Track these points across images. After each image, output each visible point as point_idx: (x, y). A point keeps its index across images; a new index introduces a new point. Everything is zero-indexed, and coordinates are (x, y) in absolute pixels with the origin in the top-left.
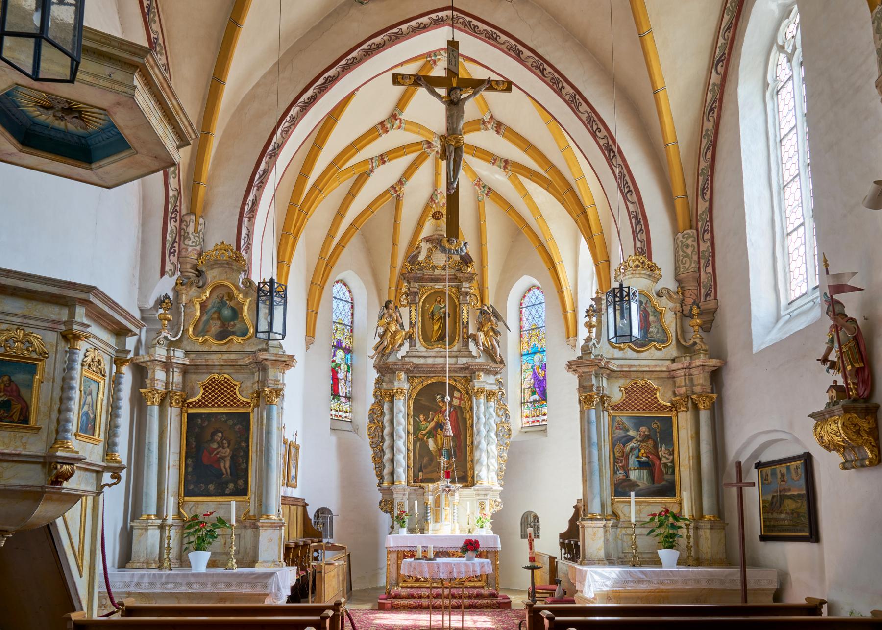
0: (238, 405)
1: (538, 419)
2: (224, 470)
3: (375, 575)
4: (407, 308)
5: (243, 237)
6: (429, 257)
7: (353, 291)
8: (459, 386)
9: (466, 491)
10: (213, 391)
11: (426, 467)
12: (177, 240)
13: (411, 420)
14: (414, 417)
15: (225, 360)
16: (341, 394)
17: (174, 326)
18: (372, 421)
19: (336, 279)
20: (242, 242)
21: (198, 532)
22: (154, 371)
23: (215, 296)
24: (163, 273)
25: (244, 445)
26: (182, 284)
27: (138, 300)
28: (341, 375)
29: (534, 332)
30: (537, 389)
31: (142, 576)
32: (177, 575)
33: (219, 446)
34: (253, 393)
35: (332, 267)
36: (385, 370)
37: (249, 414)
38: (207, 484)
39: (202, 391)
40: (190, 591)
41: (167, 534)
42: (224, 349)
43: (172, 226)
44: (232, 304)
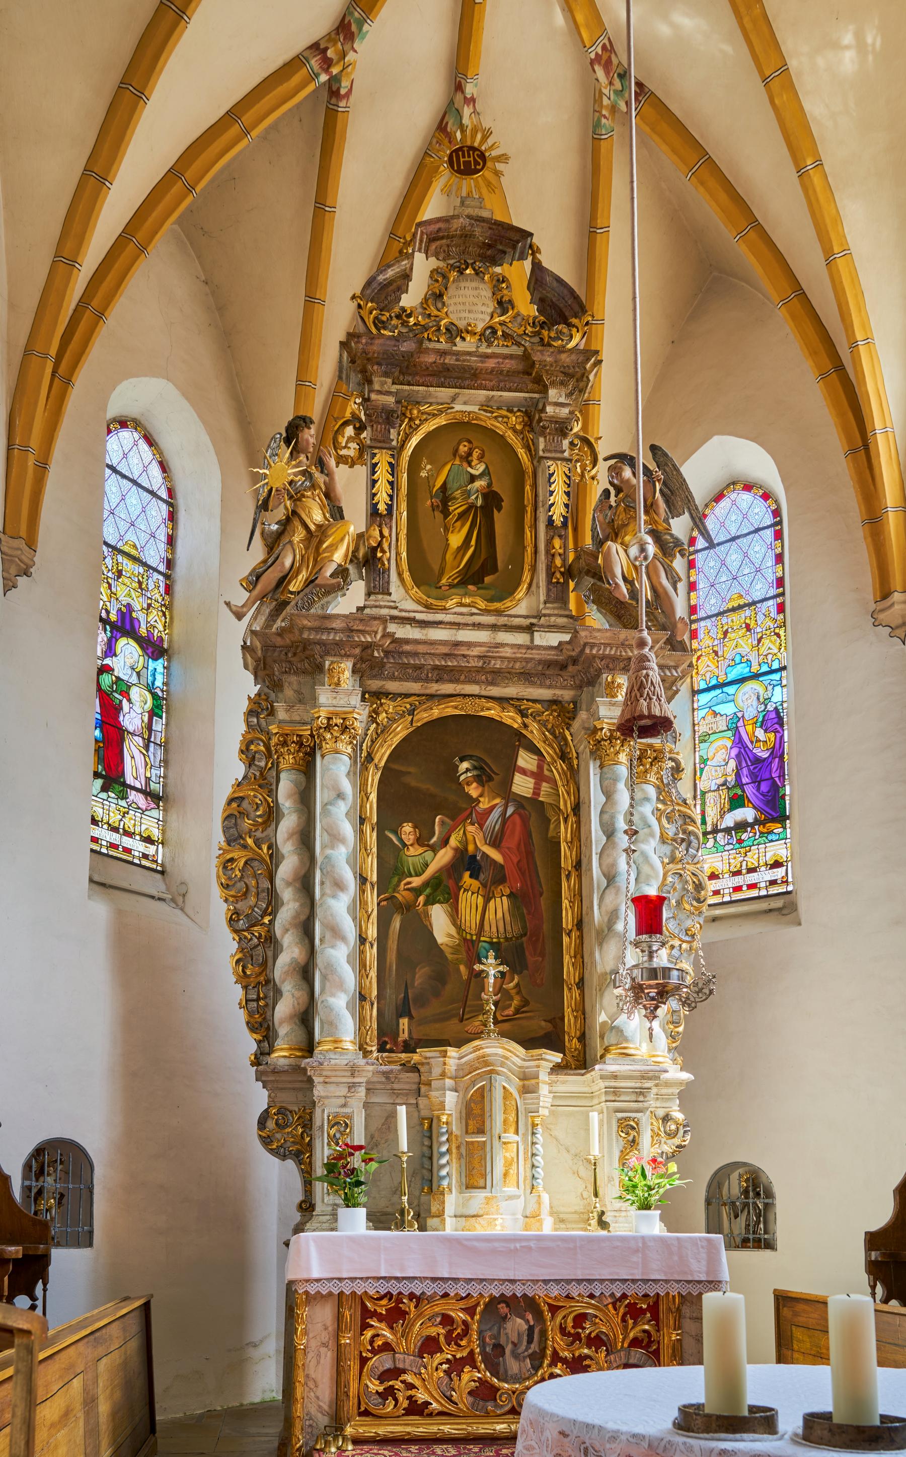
1: (752, 878)
3: (236, 1361)
4: (362, 471)
6: (436, 297)
8: (534, 733)
9: (572, 1083)
11: (422, 1001)
13: (372, 838)
14: (381, 827)
16: (129, 780)
18: (233, 838)
28: (132, 717)
29: (737, 619)
30: (750, 790)
36: (284, 658)
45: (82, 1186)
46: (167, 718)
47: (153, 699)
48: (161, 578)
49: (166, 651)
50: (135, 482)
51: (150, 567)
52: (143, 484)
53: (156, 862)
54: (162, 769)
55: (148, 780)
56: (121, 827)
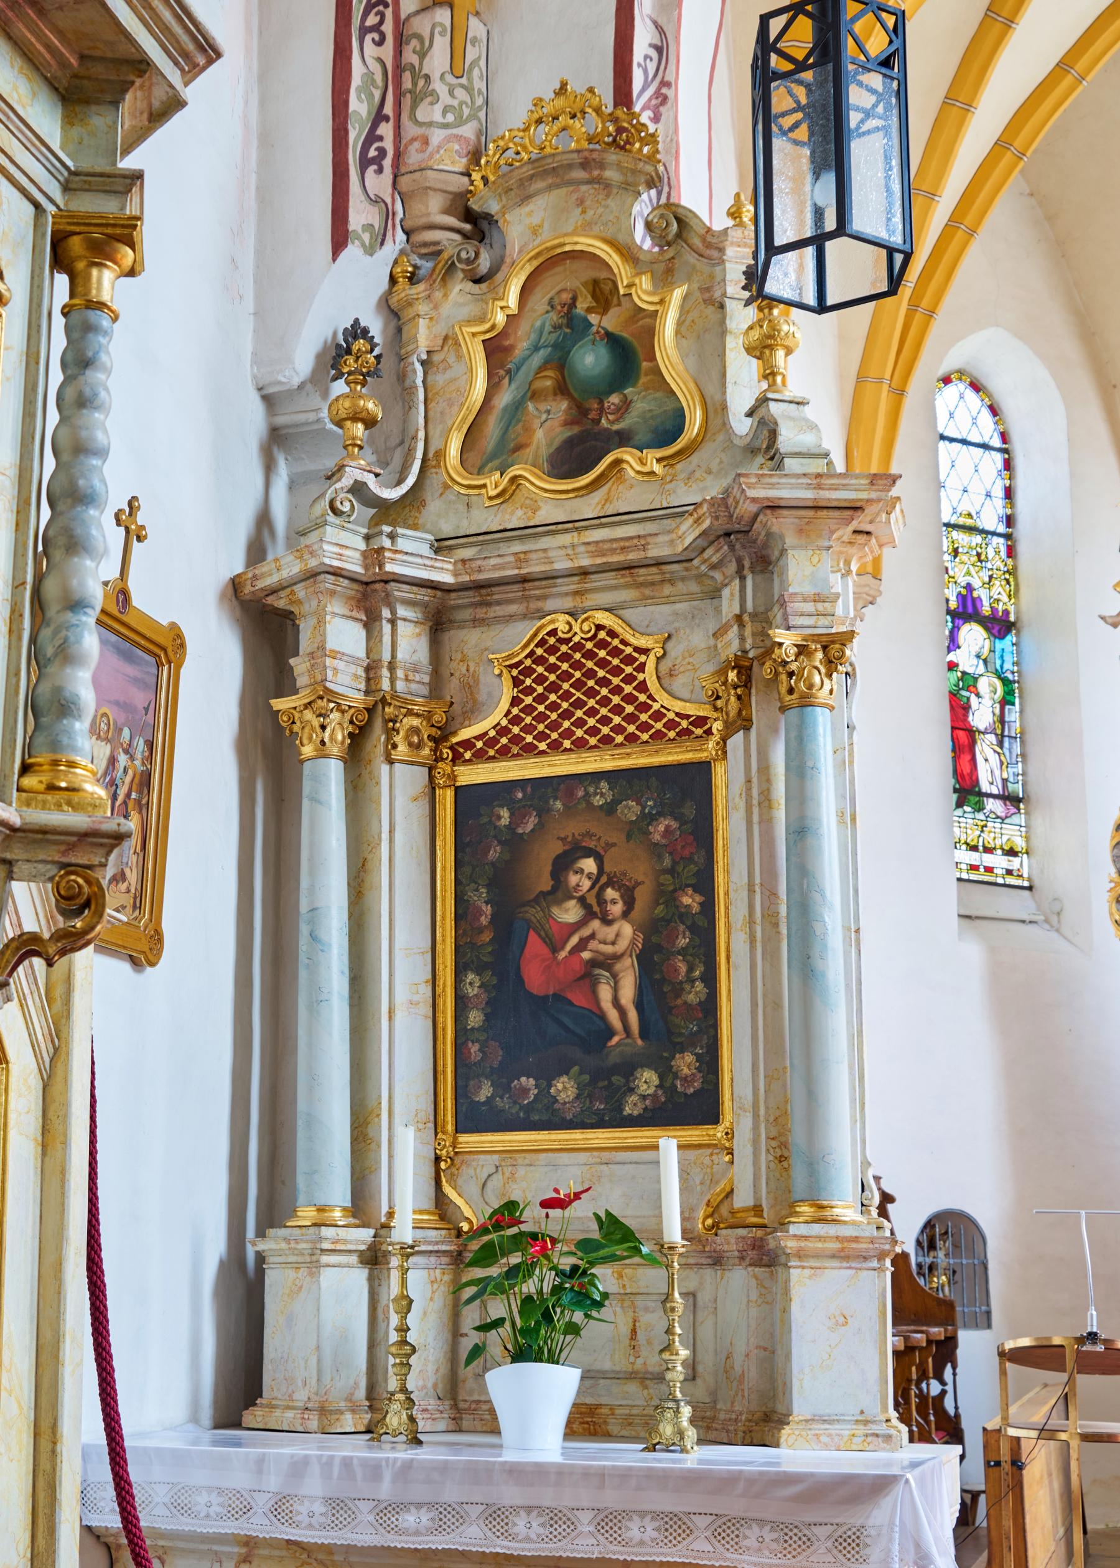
0: (658, 736)
2: (613, 1016)
5: (638, 56)
7: (1008, 406)
10: (553, 688)
12: (388, 110)
15: (597, 548)
16: (985, 787)
17: (392, 453)
19: (942, 371)
20: (638, 78)
21: (525, 1285)
22: (321, 622)
23: (539, 303)
24: (340, 239)
25: (690, 900)
26: (413, 279)
27: (256, 359)
28: (982, 716)
31: (298, 1468)
32: (444, 1468)
33: (590, 914)
34: (722, 672)
35: (931, 313)
37: (704, 769)
38: (546, 1078)
39: (507, 692)
40: (501, 1546)
41: (395, 1289)
42: (589, 507)
43: (368, 61)
44: (611, 321)
45: (976, 1262)
46: (1021, 704)
47: (1004, 685)
48: (1001, 540)
49: (1013, 624)
50: (964, 442)
51: (987, 533)
52: (974, 440)
53: (1021, 876)
54: (1020, 765)
55: (1005, 781)
56: (981, 844)
